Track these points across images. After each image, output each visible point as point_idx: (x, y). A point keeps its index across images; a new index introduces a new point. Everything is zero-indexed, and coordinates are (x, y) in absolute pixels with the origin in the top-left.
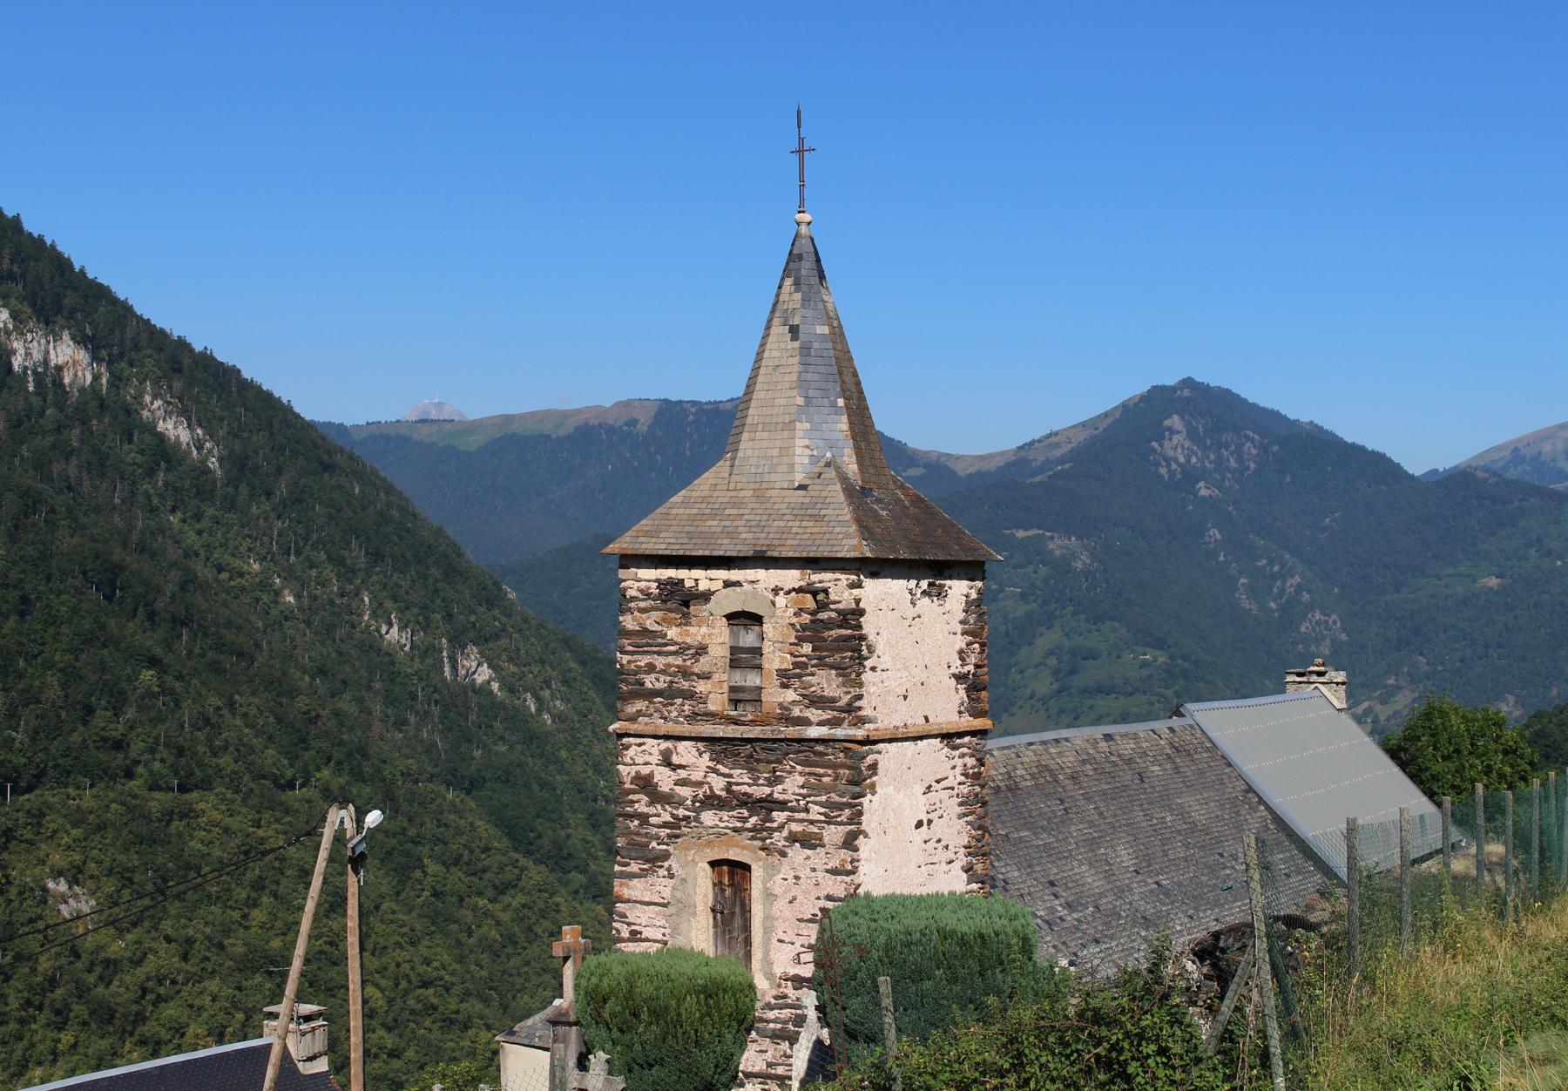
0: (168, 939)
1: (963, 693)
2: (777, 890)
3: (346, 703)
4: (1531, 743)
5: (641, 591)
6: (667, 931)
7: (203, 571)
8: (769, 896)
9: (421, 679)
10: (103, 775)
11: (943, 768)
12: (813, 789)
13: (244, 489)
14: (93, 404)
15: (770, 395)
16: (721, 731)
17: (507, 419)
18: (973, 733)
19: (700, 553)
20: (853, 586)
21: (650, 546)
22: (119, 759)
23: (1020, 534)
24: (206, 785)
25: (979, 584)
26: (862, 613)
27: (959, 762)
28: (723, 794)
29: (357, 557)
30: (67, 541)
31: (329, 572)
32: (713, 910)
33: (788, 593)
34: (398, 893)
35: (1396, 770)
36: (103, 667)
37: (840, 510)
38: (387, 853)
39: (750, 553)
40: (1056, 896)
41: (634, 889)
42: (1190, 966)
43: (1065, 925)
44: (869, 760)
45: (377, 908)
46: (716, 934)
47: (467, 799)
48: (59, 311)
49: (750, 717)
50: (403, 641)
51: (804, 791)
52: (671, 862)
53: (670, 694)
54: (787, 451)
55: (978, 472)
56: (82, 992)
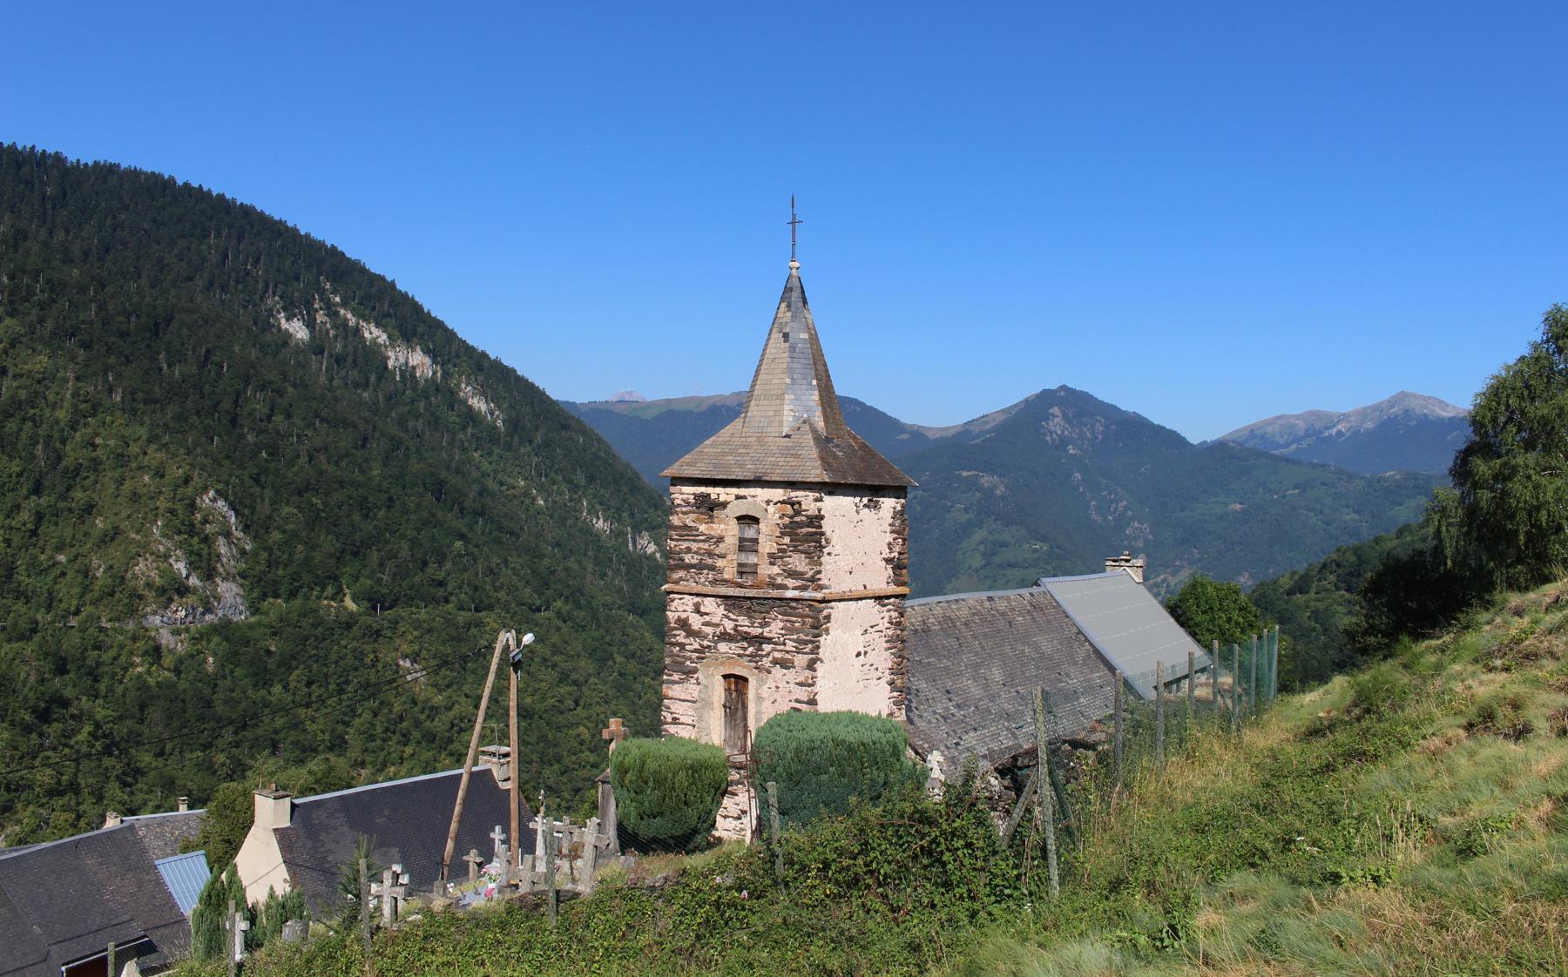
0: (467, 696)
1: (890, 571)
3: (572, 563)
4: (1256, 603)
7: (492, 485)
8: (759, 699)
10: (432, 601)
11: (876, 619)
13: (516, 439)
14: (432, 389)
16: (731, 591)
17: (670, 401)
20: (817, 500)
22: (441, 592)
23: (965, 474)
24: (490, 608)
26: (822, 517)
30: (415, 466)
31: (564, 487)
35: (1172, 620)
36: (433, 539)
37: (811, 451)
41: (675, 691)
42: (993, 781)
44: (825, 613)
48: (415, 334)
53: (700, 567)
54: (779, 413)
56: (418, 724)
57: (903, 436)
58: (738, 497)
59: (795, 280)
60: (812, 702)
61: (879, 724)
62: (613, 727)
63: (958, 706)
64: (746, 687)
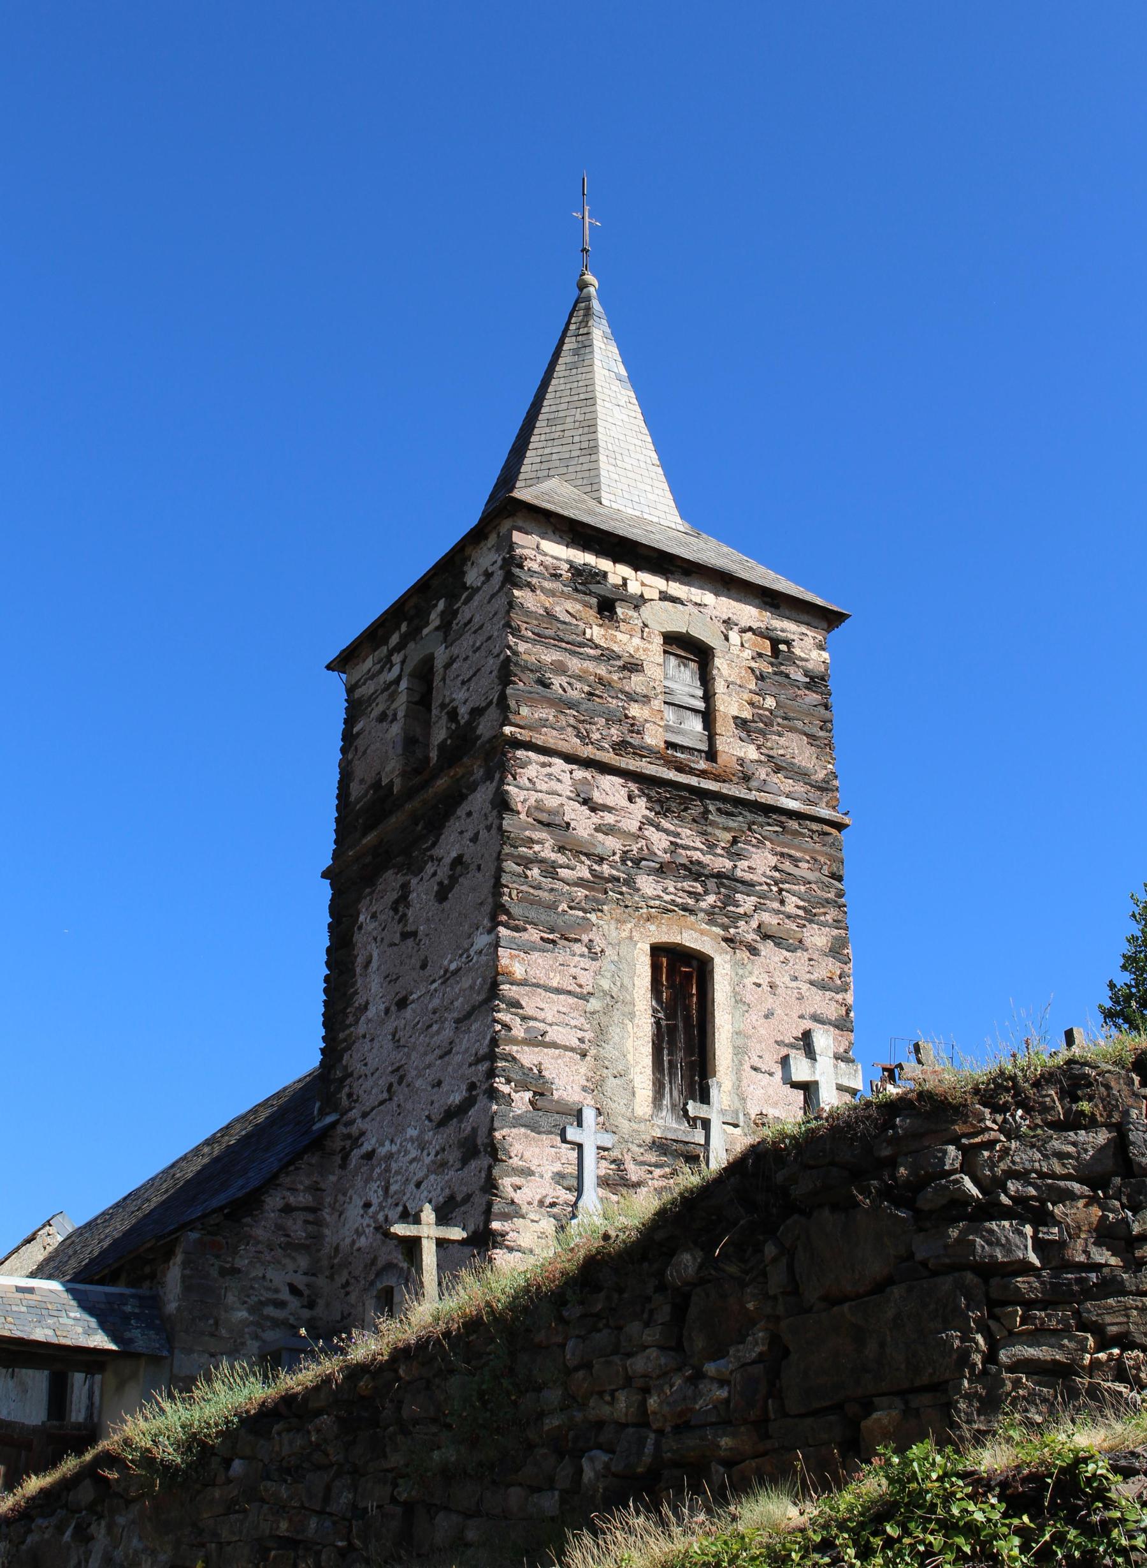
6: (588, 1035)
33: (743, 631)
58: (664, 597)
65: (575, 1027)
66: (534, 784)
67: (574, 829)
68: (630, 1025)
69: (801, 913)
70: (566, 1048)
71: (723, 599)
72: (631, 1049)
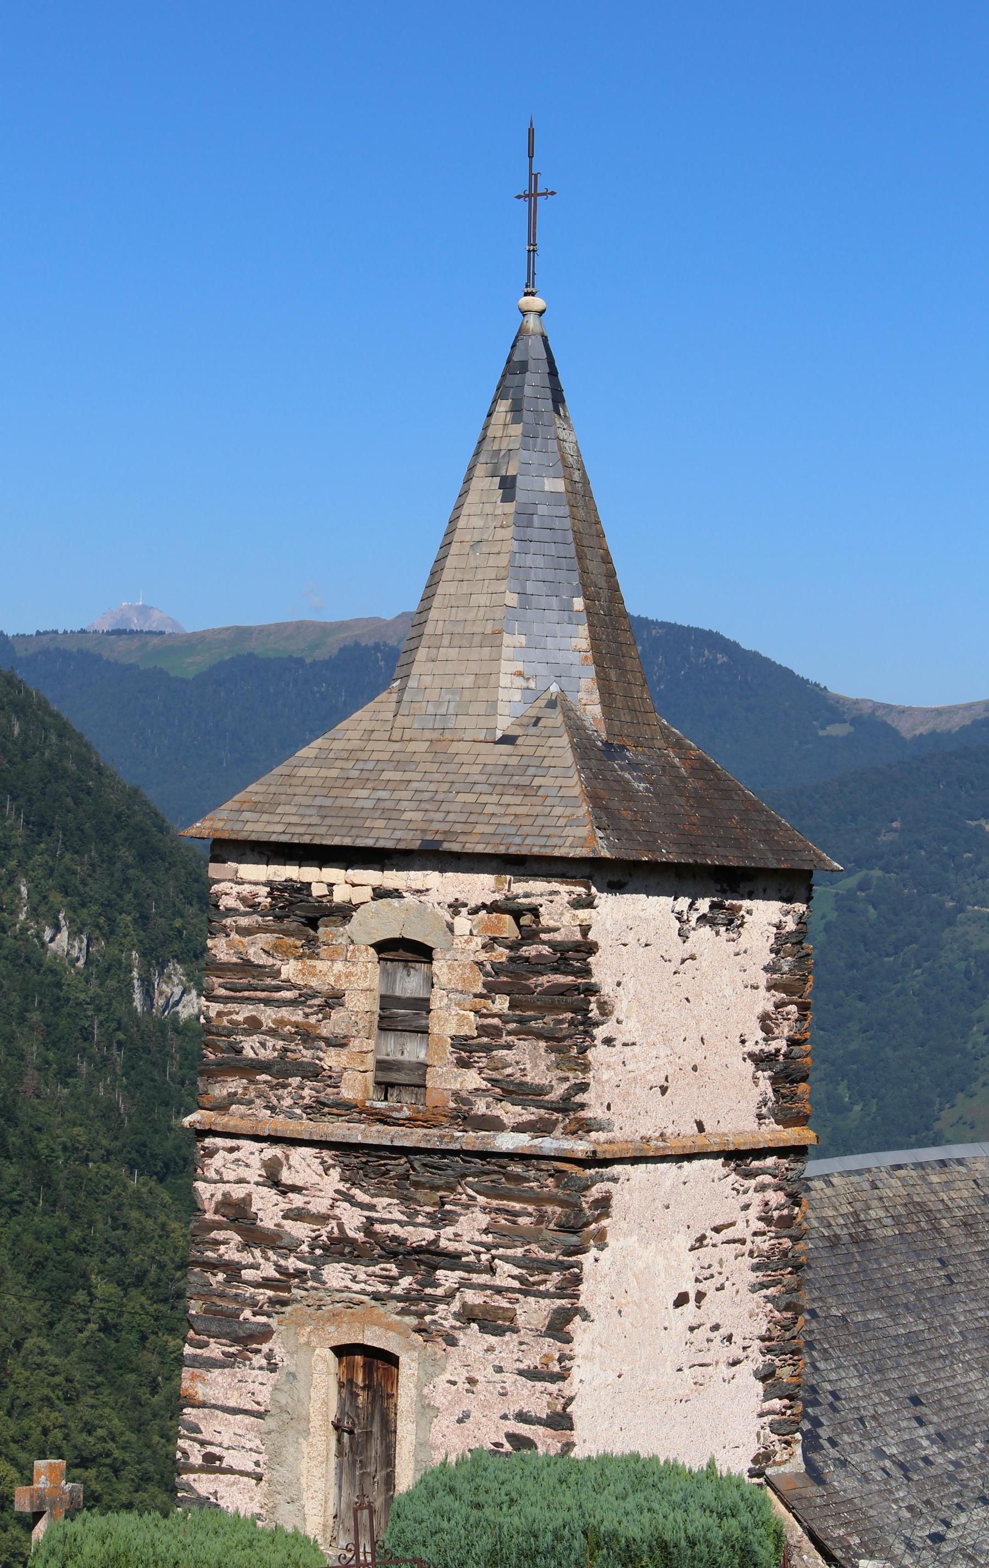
1: (765, 1086)
2: (440, 1400)
5: (243, 900)
6: (262, 1458)
8: (427, 1409)
9: (98, 1009)
11: (728, 1209)
12: (503, 1235)
15: (465, 588)
16: (360, 1133)
17: (242, 633)
18: (782, 1152)
19: (337, 841)
21: (259, 827)
25: (801, 907)
26: (591, 948)
27: (756, 1199)
28: (360, 1236)
29: (12, 828)
32: (337, 1427)
33: (475, 911)
34: (51, 1325)
37: (564, 778)
38: (38, 1264)
39: (416, 845)
40: (921, 1422)
43: (932, 1471)
44: (596, 1192)
45: (18, 1345)
46: (340, 1467)
47: (159, 1189)
49: (406, 1113)
50: (75, 953)
51: (489, 1239)
52: (274, 1344)
53: (281, 1069)
54: (486, 680)
55: (933, 734)
57: (838, 730)
58: (380, 893)
59: (536, 350)
60: (560, 1421)
61: (708, 1493)
62: (42, 1483)
63: (941, 1438)
64: (393, 1380)
65: (251, 1450)
66: (221, 1174)
67: (261, 1220)
68: (305, 1444)
69: (516, 1284)
70: (243, 1473)
71: (450, 874)
72: (305, 1472)
